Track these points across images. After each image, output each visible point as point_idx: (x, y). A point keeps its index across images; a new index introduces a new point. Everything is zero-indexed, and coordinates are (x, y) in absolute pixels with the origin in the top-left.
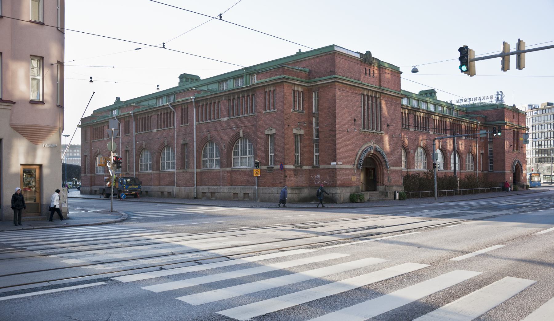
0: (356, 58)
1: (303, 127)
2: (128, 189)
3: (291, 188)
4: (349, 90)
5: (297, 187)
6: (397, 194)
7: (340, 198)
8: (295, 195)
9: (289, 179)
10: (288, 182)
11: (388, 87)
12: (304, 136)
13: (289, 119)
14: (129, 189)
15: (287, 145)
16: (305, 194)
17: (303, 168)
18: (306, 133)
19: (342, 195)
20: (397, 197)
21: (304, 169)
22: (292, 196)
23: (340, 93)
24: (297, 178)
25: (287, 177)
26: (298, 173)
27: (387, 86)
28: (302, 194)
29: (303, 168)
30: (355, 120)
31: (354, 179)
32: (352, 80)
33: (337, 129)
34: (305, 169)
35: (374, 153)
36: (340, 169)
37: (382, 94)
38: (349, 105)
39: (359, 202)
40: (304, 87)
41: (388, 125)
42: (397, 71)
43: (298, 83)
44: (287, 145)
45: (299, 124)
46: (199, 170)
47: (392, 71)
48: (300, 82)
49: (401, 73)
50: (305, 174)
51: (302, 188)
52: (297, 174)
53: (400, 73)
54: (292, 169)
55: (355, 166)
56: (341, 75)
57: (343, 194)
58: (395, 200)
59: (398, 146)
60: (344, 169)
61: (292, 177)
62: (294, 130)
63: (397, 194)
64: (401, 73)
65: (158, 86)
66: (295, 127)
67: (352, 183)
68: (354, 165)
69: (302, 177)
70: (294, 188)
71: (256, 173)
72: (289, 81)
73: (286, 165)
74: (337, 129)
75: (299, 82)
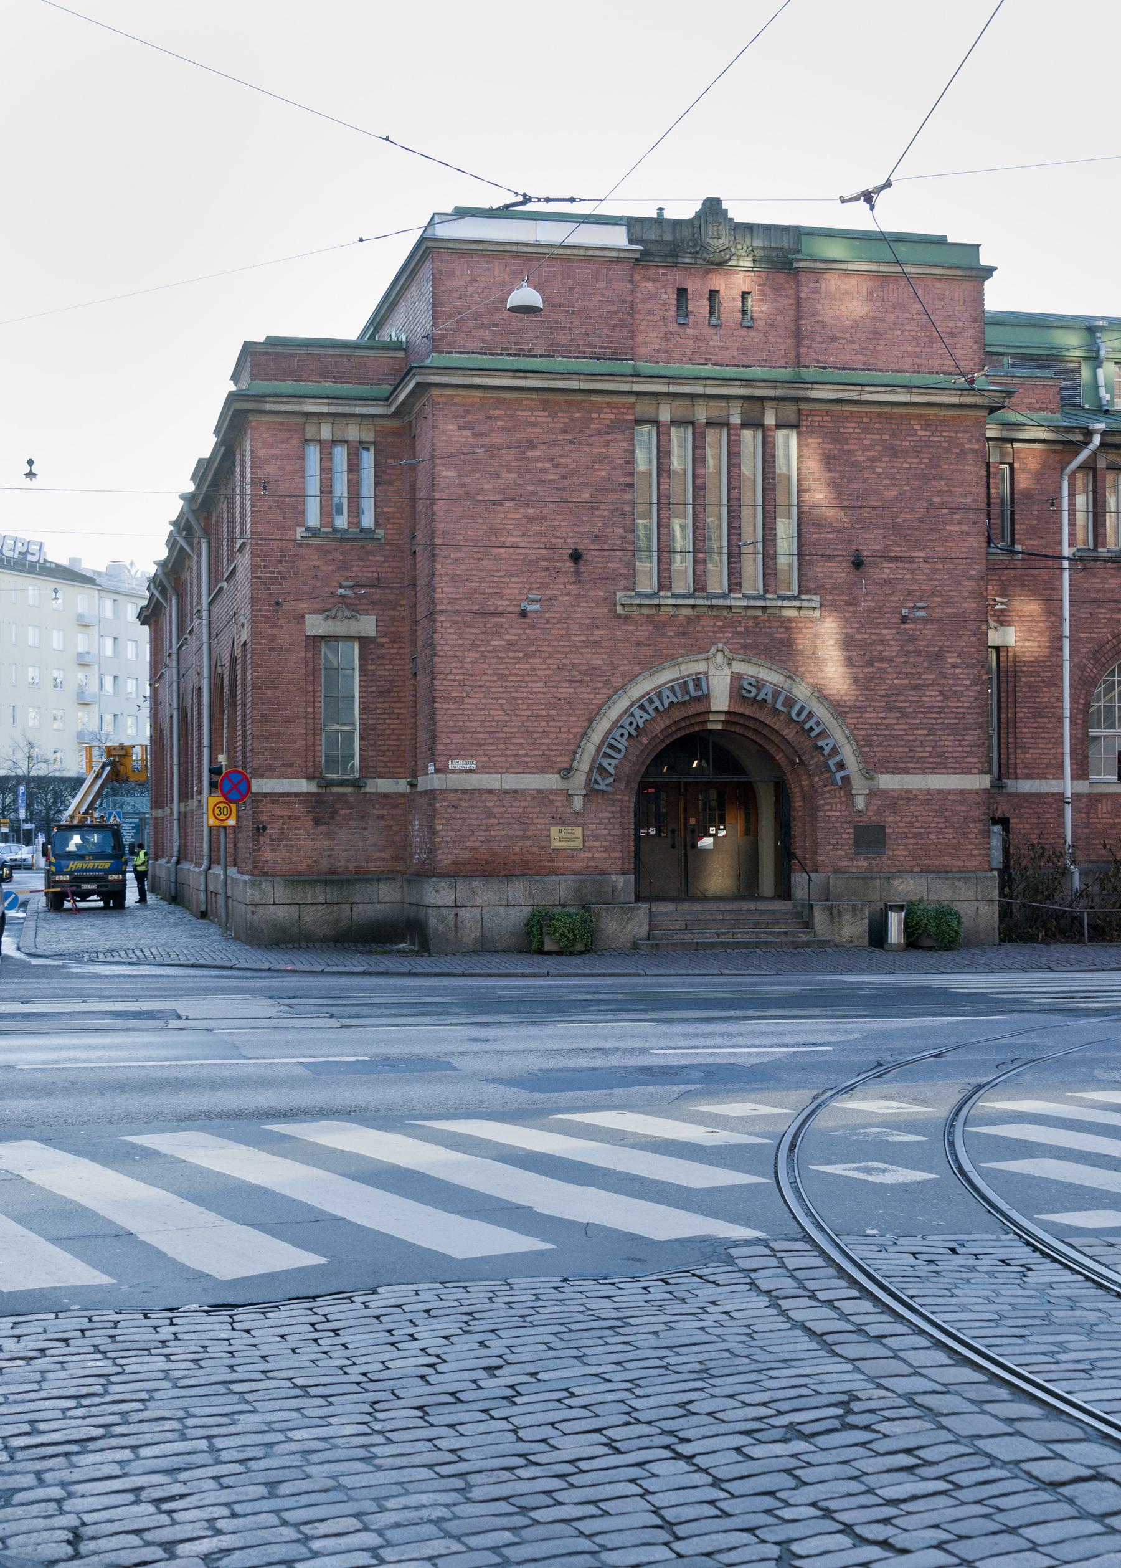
0: (590, 253)
1: (374, 603)
2: (65, 874)
3: (286, 881)
4: (542, 417)
5: (335, 877)
6: (895, 921)
7: (456, 931)
8: (310, 909)
9: (279, 840)
10: (272, 851)
11: (860, 365)
12: (382, 646)
13: (279, 572)
14: (70, 873)
15: (268, 688)
16: (378, 906)
17: (368, 790)
18: (392, 629)
19: (466, 914)
20: (895, 932)
21: (377, 794)
22: (296, 915)
23: (467, 433)
24: (330, 835)
25: (264, 828)
26: (335, 812)
27: (859, 361)
28: (358, 909)
29: (368, 790)
30: (576, 556)
31: (559, 838)
32: (559, 363)
33: (439, 608)
34: (386, 796)
35: (736, 710)
36: (464, 791)
37: (803, 406)
38: (530, 488)
39: (549, 953)
40: (382, 422)
41: (858, 563)
42: (972, 269)
43: (324, 409)
44: (269, 692)
45: (340, 591)
46: (1083, 787)
47: (874, 275)
48: (335, 401)
49: (989, 271)
50: (382, 817)
51: (357, 881)
52: (332, 818)
53: (981, 274)
54: (297, 795)
55: (579, 780)
56: (471, 345)
57: (478, 910)
58: (879, 953)
59: (954, 666)
60: (490, 792)
61: (297, 828)
62: (309, 618)
63: (895, 921)
64: (989, 271)
65: (30, 462)
66: (317, 607)
67: (552, 861)
68: (567, 772)
69: (365, 829)
70: (305, 881)
71: (217, 811)
72: (268, 407)
73: (262, 776)
74: (439, 608)
75: (329, 404)
